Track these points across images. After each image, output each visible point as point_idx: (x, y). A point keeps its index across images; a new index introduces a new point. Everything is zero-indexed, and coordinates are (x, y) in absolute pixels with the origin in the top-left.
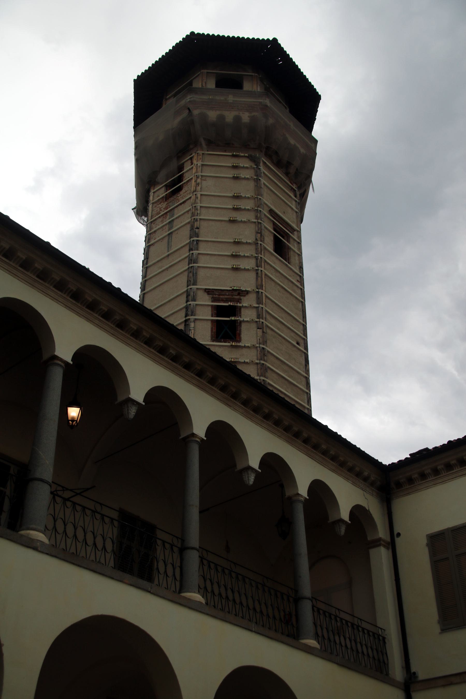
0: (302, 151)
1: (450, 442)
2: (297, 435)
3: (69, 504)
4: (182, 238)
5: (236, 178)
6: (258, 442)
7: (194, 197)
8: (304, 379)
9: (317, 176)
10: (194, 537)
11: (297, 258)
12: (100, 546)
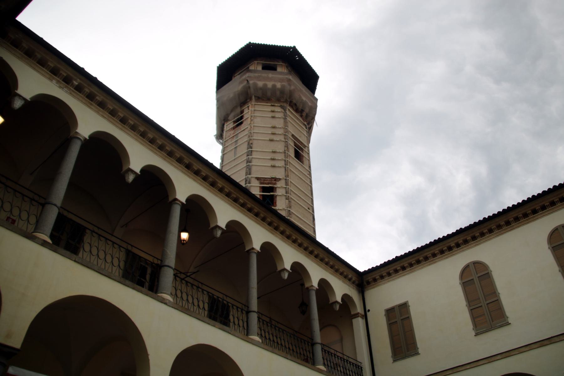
0: (310, 104)
1: (396, 257)
2: (311, 253)
3: (184, 282)
4: (243, 149)
5: (273, 117)
6: (289, 255)
7: (249, 127)
8: (312, 229)
9: (317, 118)
10: (254, 305)
11: (307, 161)
12: (201, 306)
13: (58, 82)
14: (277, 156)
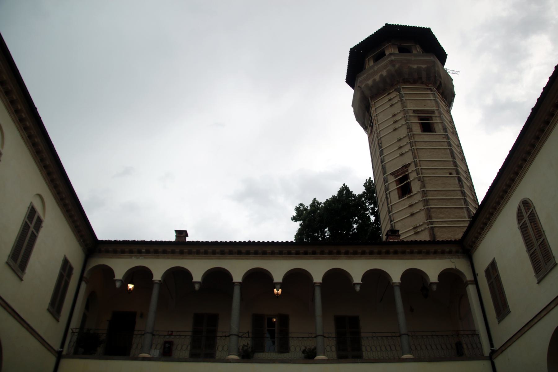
13: (135, 256)
14: (402, 143)
